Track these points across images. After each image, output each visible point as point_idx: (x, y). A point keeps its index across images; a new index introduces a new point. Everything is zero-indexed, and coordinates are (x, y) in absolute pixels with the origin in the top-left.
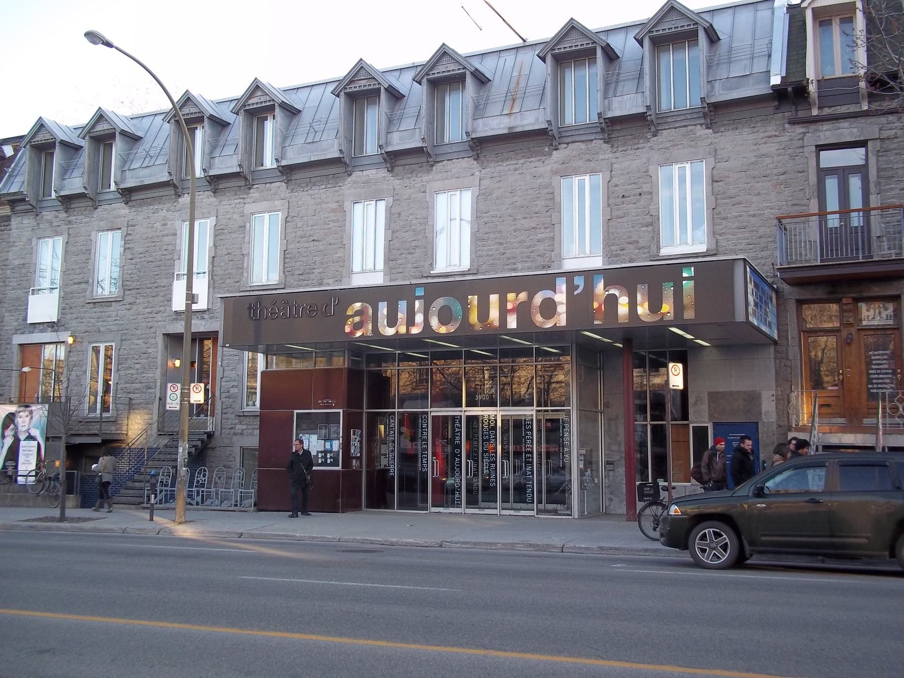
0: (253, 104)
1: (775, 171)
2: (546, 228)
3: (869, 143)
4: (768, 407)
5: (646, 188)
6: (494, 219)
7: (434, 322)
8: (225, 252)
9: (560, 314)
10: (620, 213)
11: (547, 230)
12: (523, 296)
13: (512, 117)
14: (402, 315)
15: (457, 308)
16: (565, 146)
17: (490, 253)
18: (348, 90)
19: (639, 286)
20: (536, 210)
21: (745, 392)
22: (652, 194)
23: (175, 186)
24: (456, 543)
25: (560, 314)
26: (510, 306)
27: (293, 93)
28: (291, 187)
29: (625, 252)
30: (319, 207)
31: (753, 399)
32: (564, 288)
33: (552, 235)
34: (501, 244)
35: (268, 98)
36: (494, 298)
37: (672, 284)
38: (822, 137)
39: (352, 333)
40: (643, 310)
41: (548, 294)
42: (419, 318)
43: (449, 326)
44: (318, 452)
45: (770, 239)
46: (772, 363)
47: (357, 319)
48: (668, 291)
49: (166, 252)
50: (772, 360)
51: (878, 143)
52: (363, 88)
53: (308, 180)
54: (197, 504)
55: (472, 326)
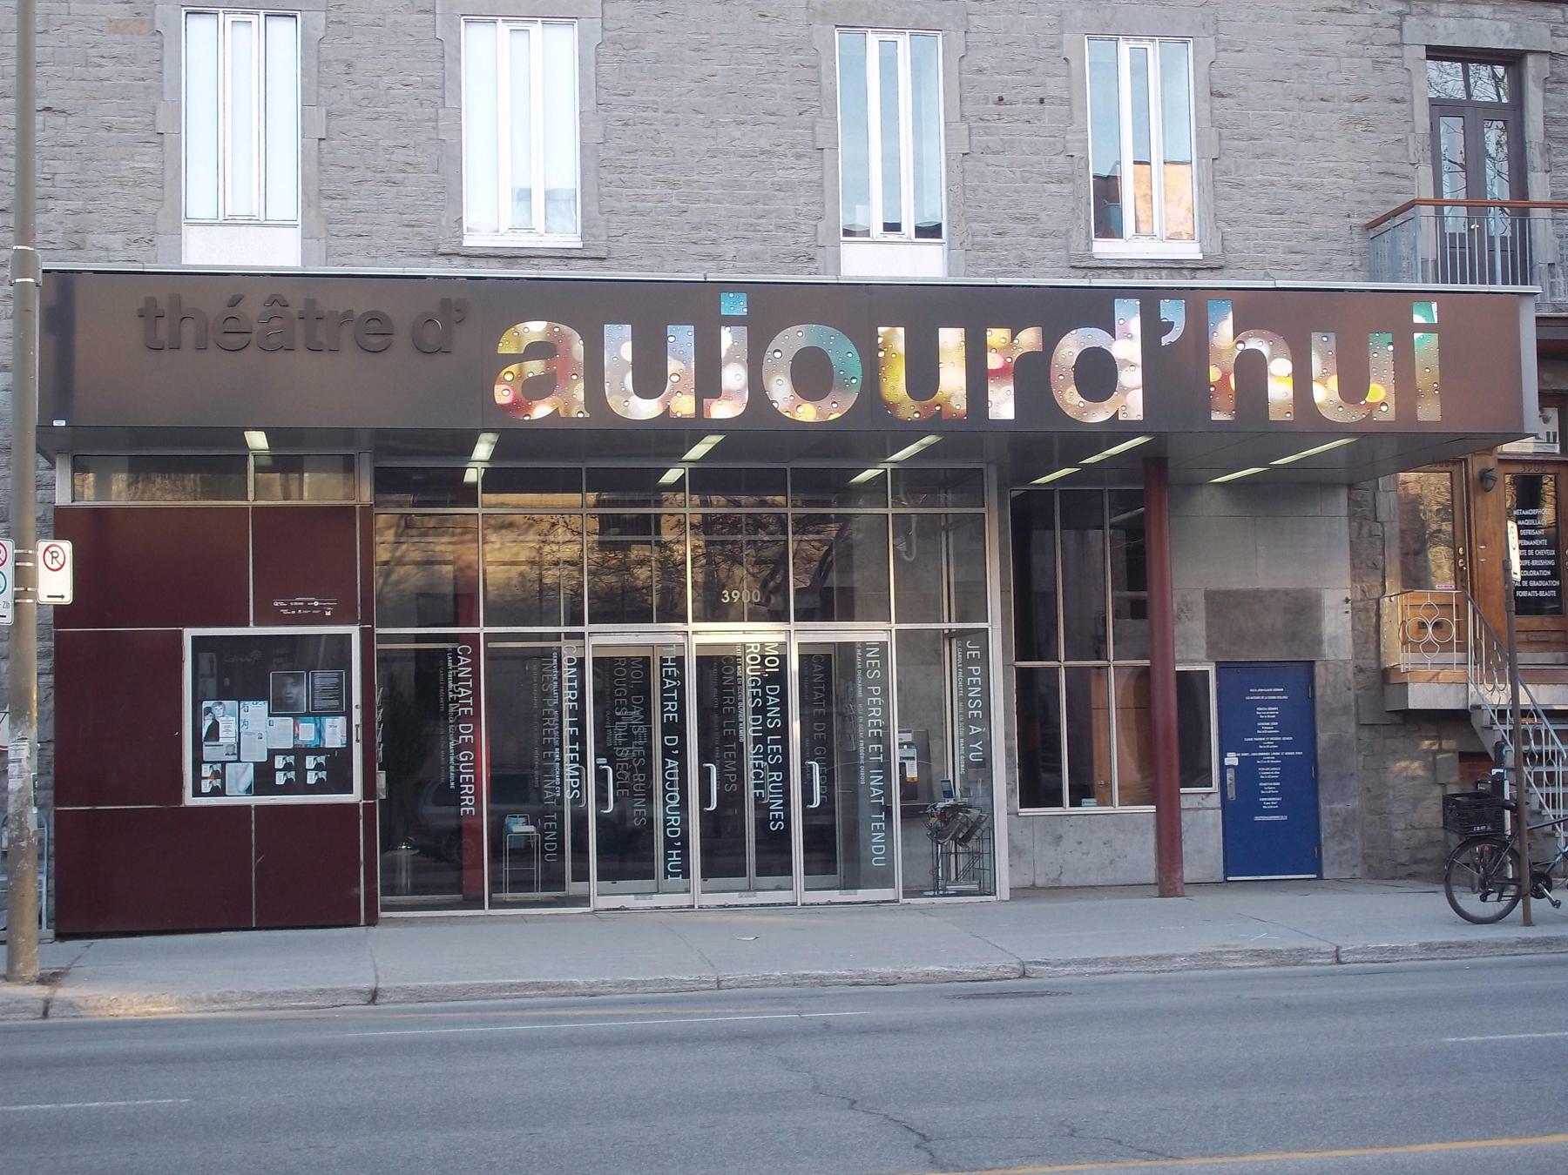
1: (1346, 92)
2: (799, 157)
3: (1530, 60)
4: (1336, 625)
5: (1054, 88)
6: (650, 114)
7: (781, 391)
9: (1126, 391)
11: (804, 162)
12: (1029, 338)
14: (680, 364)
15: (844, 356)
19: (1315, 337)
21: (1286, 592)
22: (1070, 103)
24: (1067, 964)
25: (1126, 391)
26: (994, 361)
29: (1007, 239)
31: (1304, 608)
32: (1135, 325)
33: (815, 176)
34: (673, 185)
36: (951, 339)
37: (1389, 337)
38: (1441, 29)
39: (519, 406)
40: (1325, 392)
41: (1092, 337)
42: (734, 376)
43: (825, 403)
44: (272, 753)
45: (1336, 246)
46: (1342, 528)
47: (535, 368)
48: (1382, 352)
50: (1345, 521)
51: (1546, 62)
55: (894, 407)
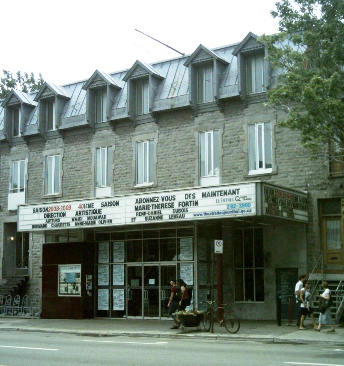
0: (45, 96)
2: (191, 161)
8: (33, 177)
10: (228, 152)
13: (173, 99)
16: (201, 114)
17: (164, 175)
18: (91, 87)
20: (187, 151)
23: (8, 142)
27: (159, 67)
28: (65, 141)
29: (231, 174)
30: (79, 151)
35: (52, 93)
49: (4, 178)
52: (98, 86)
53: (74, 137)
54: (14, 315)
